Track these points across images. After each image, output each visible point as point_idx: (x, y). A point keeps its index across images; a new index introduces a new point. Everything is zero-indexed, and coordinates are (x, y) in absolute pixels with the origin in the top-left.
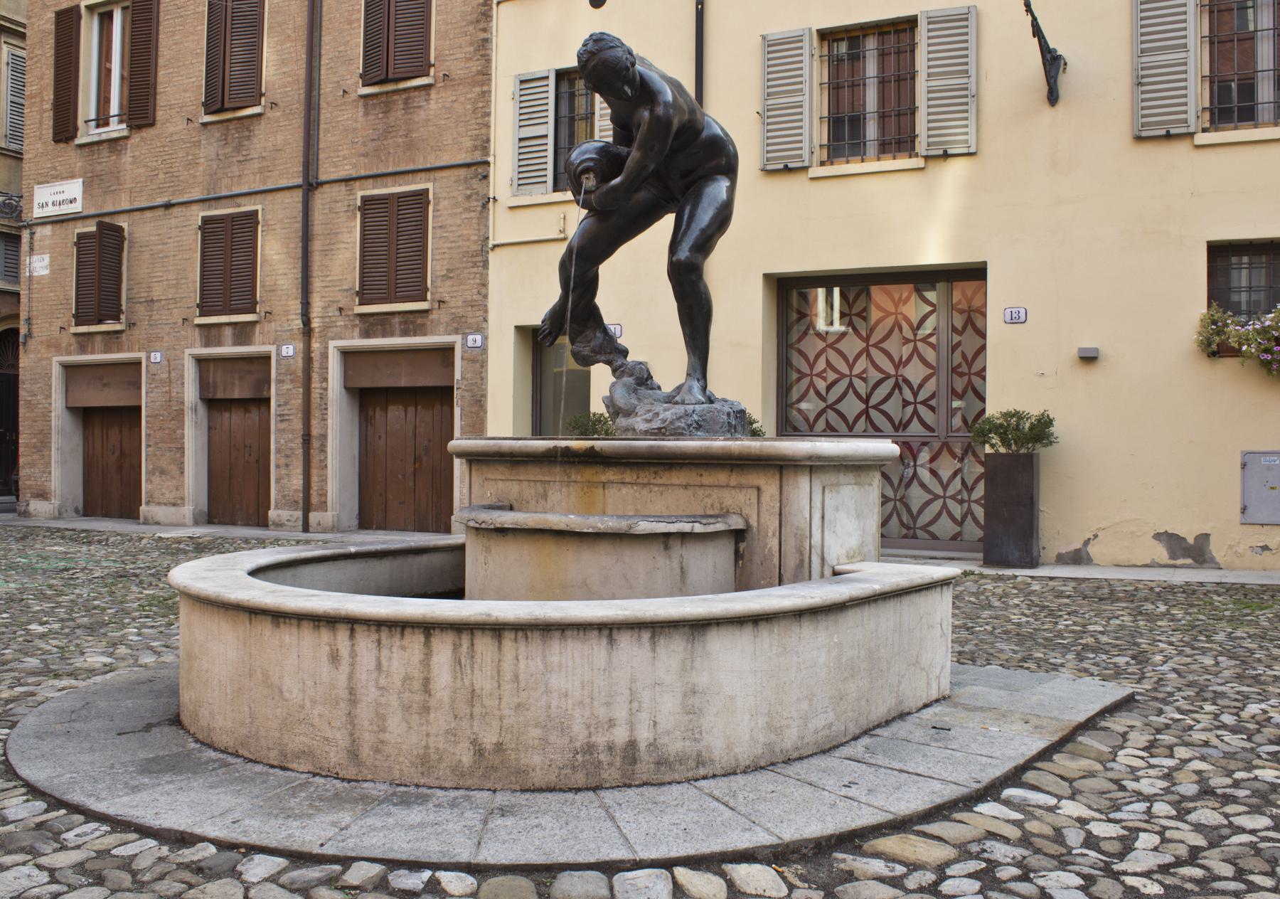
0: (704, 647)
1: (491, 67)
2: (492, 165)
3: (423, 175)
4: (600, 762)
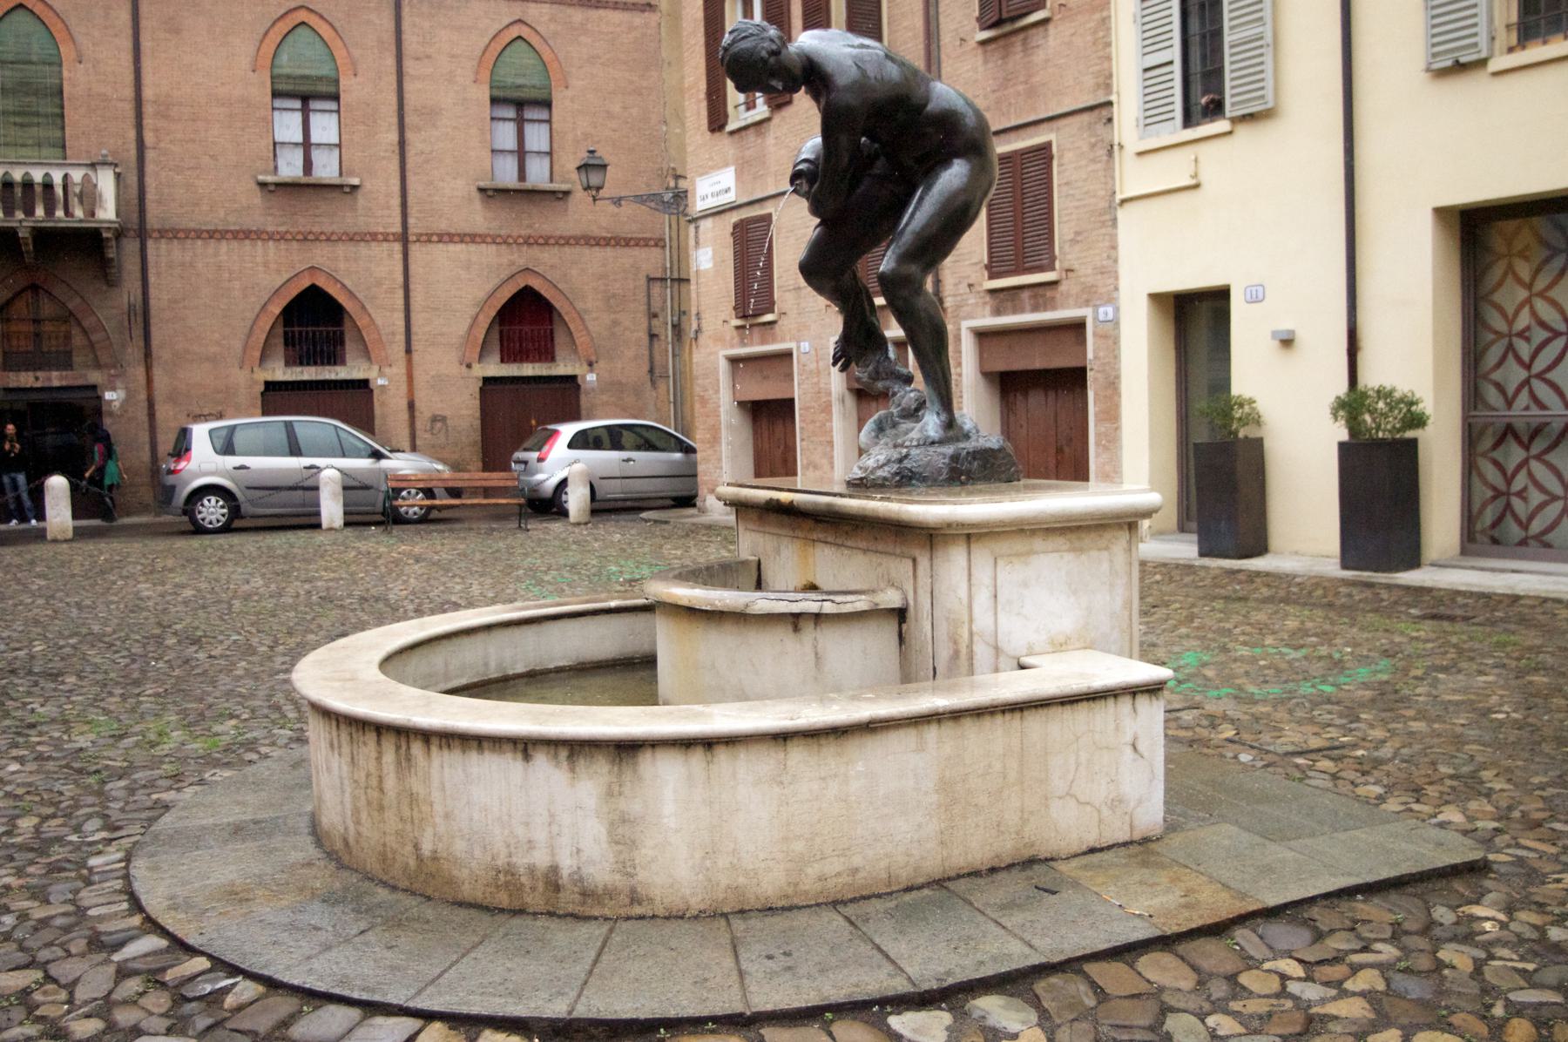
0: (635, 771)
2: (1115, 106)
4: (522, 885)
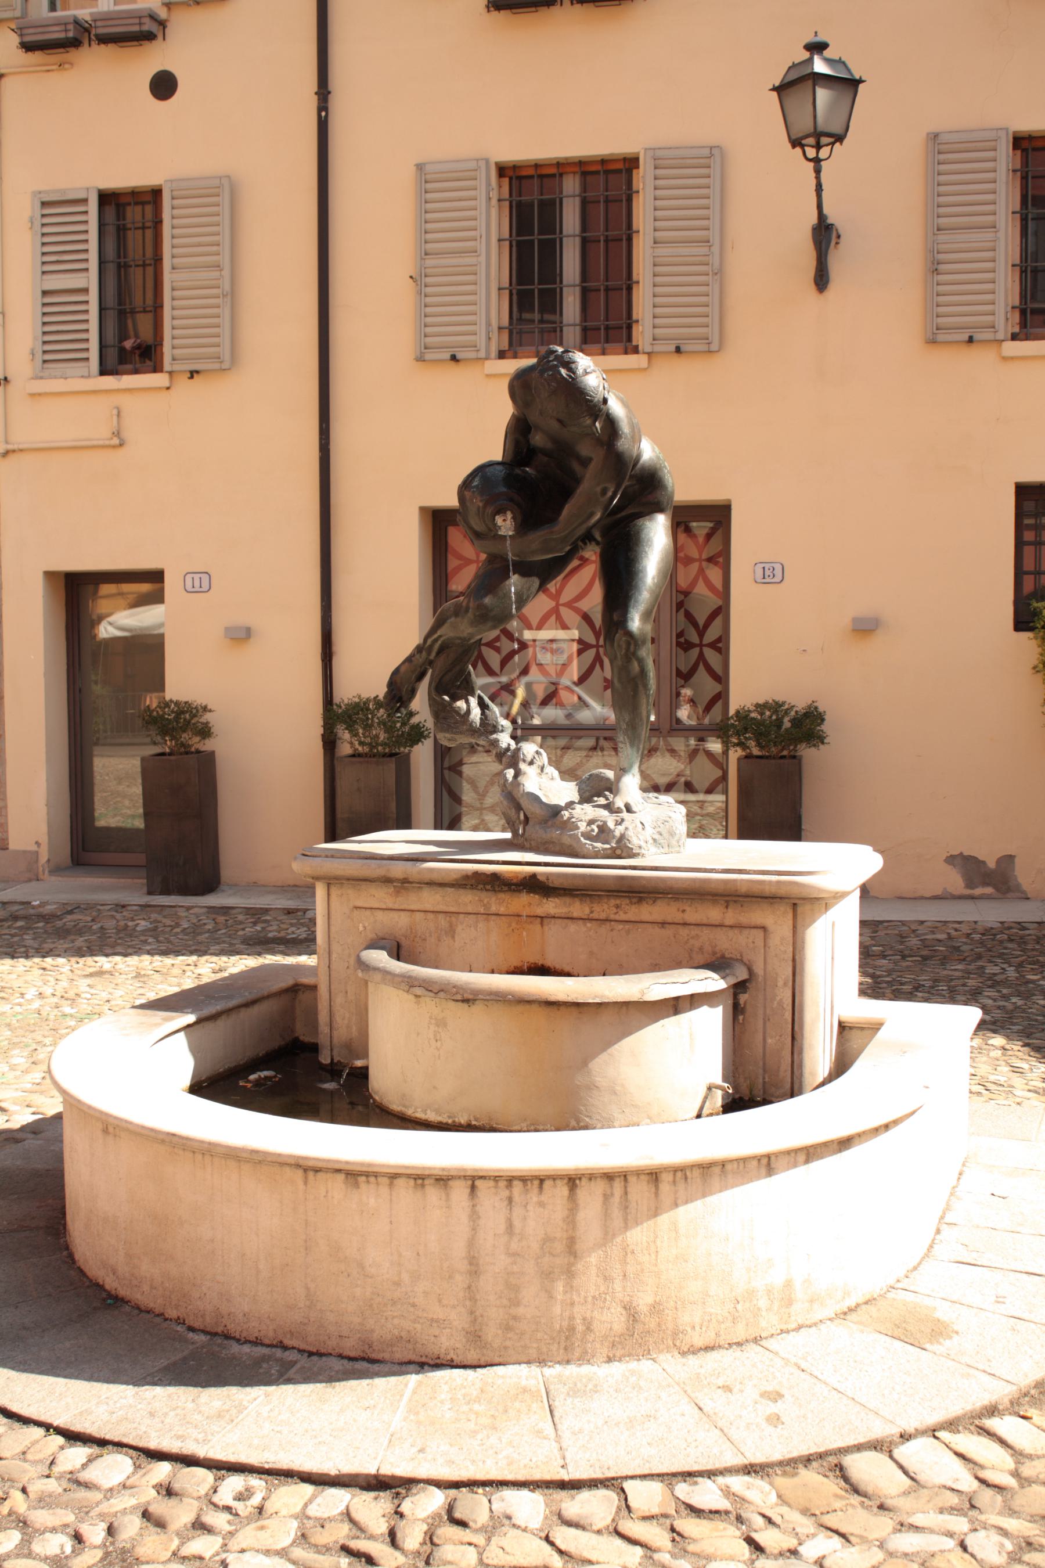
4: (759, 1309)
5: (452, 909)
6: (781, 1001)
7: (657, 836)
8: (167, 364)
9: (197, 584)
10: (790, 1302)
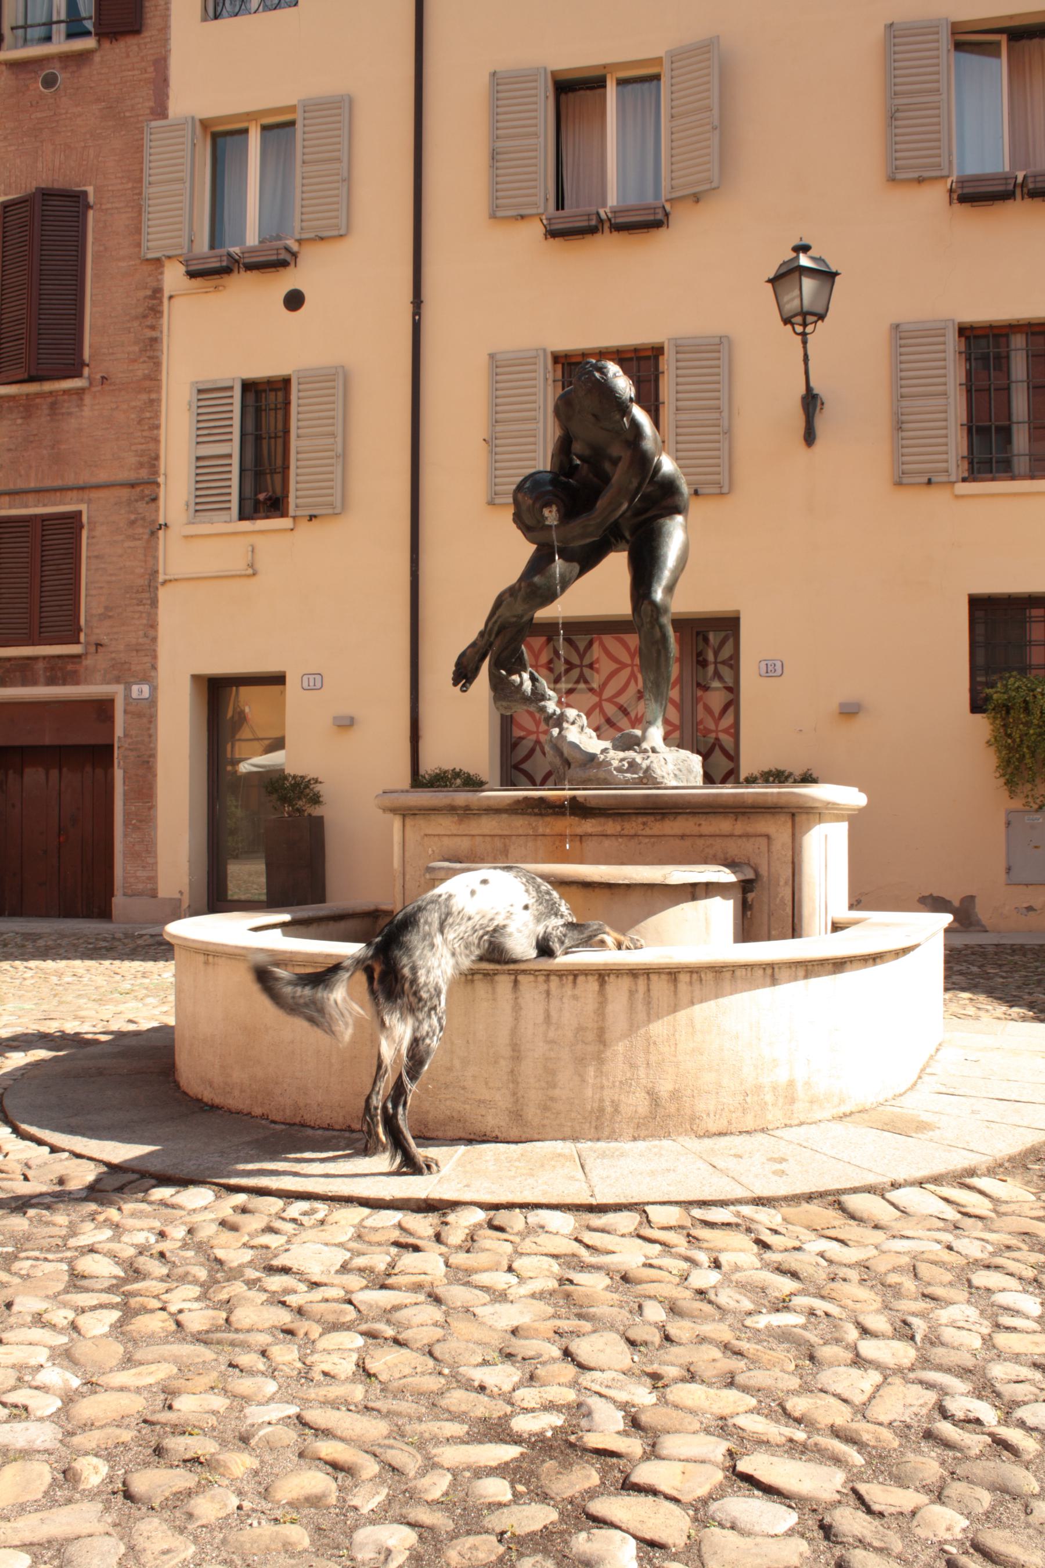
1: (160, 372)
2: (162, 487)
3: (74, 494)
4: (766, 1103)
5: (506, 833)
6: (782, 899)
7: (677, 772)
8: (292, 511)
9: (312, 684)
10: (792, 1101)
